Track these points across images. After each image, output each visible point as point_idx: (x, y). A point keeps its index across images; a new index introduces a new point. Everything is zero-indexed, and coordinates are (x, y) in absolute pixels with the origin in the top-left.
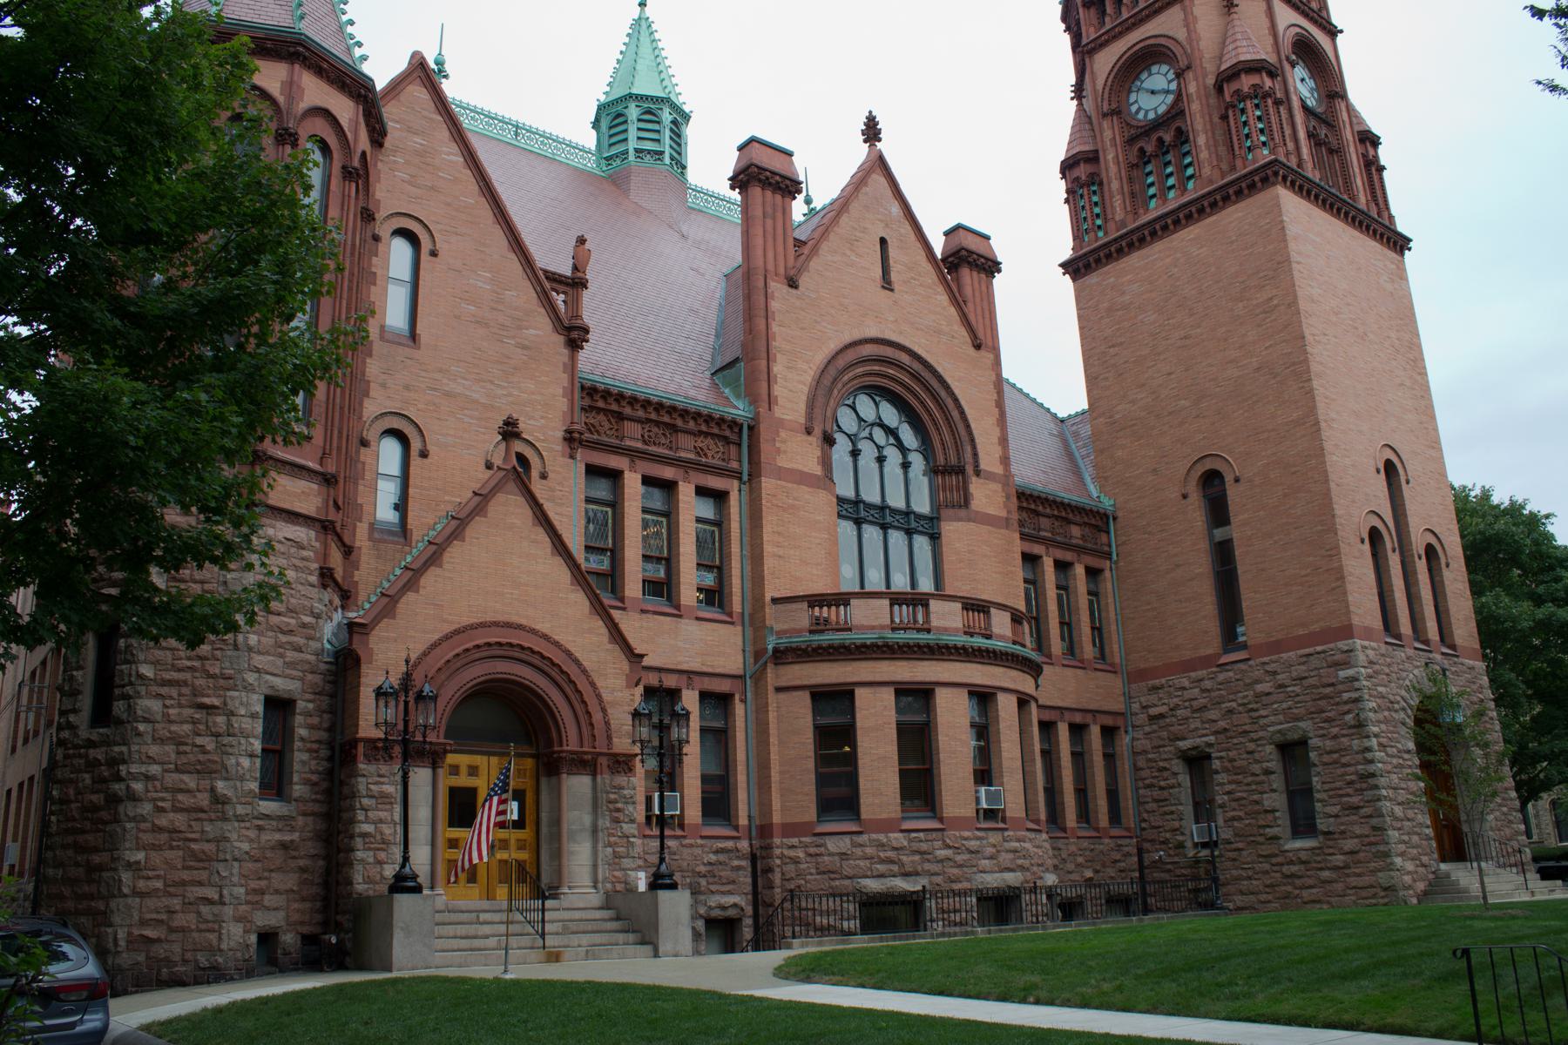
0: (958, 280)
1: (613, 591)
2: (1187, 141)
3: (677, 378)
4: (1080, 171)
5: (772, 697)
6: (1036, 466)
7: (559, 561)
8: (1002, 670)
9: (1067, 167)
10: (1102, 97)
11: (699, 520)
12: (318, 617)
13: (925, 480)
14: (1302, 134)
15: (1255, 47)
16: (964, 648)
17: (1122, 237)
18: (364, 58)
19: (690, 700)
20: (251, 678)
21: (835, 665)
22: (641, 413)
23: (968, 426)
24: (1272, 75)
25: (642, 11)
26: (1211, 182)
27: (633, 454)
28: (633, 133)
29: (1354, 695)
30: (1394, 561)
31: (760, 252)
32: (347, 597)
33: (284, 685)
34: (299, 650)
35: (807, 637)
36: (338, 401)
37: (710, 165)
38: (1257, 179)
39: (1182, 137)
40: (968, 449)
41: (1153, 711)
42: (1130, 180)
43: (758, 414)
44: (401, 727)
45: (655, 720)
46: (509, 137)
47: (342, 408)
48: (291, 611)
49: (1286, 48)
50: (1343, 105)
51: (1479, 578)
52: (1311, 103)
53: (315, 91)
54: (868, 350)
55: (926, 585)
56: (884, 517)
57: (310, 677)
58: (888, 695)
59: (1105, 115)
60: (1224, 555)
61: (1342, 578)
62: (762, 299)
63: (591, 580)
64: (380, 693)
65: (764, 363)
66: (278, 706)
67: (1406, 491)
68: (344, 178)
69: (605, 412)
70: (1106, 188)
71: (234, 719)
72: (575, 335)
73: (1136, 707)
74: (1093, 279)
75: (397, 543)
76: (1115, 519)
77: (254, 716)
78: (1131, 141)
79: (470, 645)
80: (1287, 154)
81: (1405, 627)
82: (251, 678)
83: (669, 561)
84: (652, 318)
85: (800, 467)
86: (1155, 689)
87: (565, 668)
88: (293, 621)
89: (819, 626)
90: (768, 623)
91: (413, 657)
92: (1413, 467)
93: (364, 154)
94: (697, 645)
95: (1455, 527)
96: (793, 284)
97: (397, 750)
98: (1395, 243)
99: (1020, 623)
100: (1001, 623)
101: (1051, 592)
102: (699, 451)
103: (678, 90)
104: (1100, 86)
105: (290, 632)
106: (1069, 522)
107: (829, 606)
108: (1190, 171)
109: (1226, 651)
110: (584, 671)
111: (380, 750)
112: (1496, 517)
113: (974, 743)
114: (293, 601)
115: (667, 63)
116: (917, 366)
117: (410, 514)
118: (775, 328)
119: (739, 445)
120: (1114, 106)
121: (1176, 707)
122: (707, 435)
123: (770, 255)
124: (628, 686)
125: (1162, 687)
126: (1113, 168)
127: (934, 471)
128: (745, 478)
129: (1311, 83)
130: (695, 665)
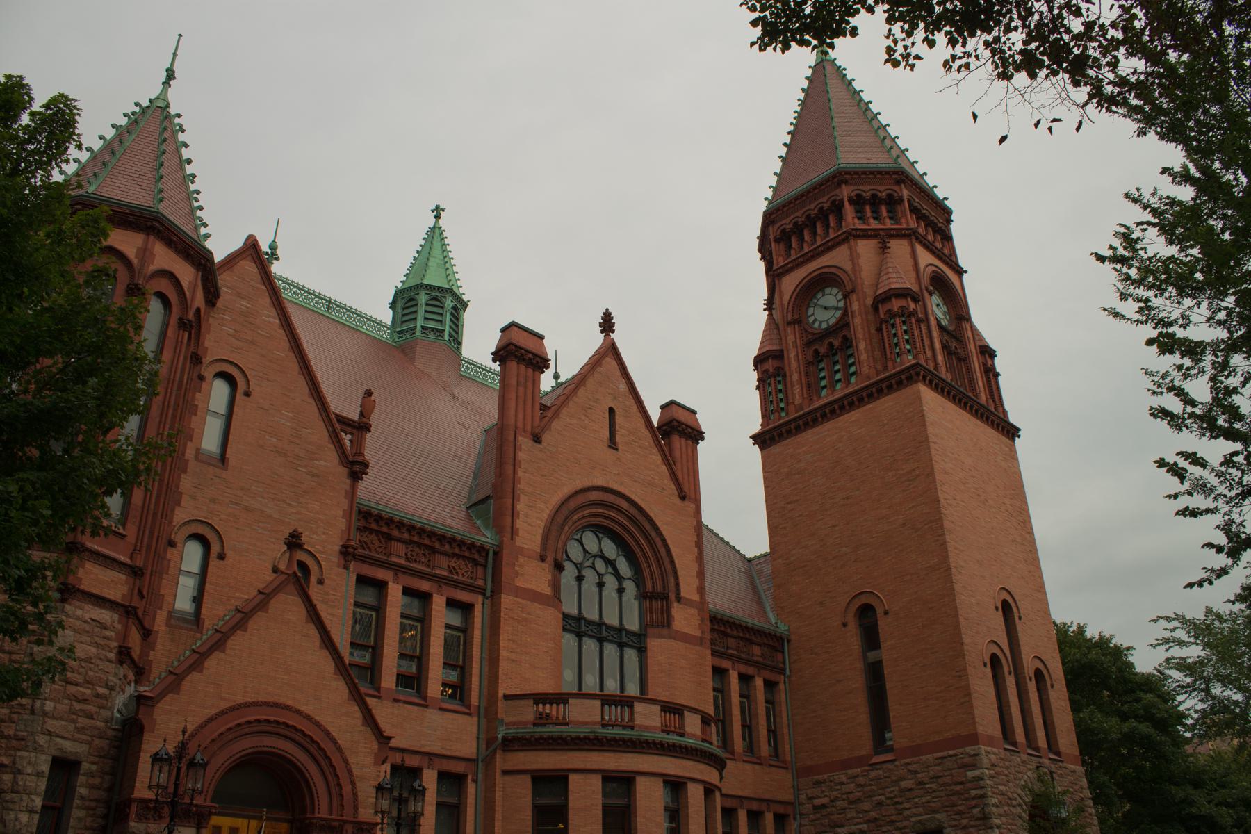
0: (669, 444)
1: (372, 682)
2: (851, 346)
3: (439, 510)
4: (768, 364)
5: (499, 779)
6: (726, 597)
7: (326, 653)
8: (691, 763)
9: (759, 362)
10: (786, 311)
11: (447, 626)
12: (111, 688)
13: (636, 604)
14: (937, 346)
15: (906, 281)
16: (661, 743)
17: (799, 417)
18: (207, 236)
19: (429, 779)
20: (42, 740)
21: (552, 753)
22: (406, 536)
23: (672, 561)
24: (915, 300)
25: (437, 222)
26: (869, 378)
27: (398, 569)
28: (421, 314)
29: (979, 792)
30: (1010, 682)
31: (512, 412)
32: (140, 673)
33: (71, 747)
34: (90, 716)
35: (532, 729)
36: (152, 507)
37: (479, 344)
38: (903, 377)
39: (847, 343)
40: (672, 580)
41: (817, 802)
42: (807, 374)
43: (501, 542)
44: (171, 789)
45: (396, 793)
46: (323, 309)
47: (155, 514)
48: (88, 682)
49: (926, 280)
50: (968, 326)
51: (1078, 697)
52: (944, 322)
53: (163, 257)
54: (595, 496)
55: (632, 689)
56: (600, 632)
57: (97, 741)
58: (596, 781)
59: (789, 323)
60: (875, 674)
61: (969, 694)
62: (511, 450)
63: (354, 673)
64: (156, 758)
65: (509, 501)
66: (64, 767)
67: (1019, 625)
68: (180, 328)
69: (375, 531)
70: (788, 379)
71: (20, 777)
72: (357, 468)
73: (803, 797)
74: (776, 449)
75: (191, 630)
76: (789, 641)
77: (39, 775)
78: (808, 344)
79: (242, 721)
80: (926, 360)
81: (1020, 737)
82: (42, 740)
83: (421, 660)
84: (422, 460)
85: (534, 588)
86: (818, 783)
87: (322, 745)
88: (89, 692)
89: (542, 720)
90: (499, 716)
91: (190, 728)
92: (1024, 606)
93: (198, 310)
94: (441, 732)
95: (1057, 656)
96: (537, 439)
97: (166, 811)
98: (1008, 431)
99: (709, 725)
100: (692, 724)
101: (735, 699)
102: (452, 570)
103: (459, 283)
104: (786, 303)
105: (85, 701)
106: (752, 642)
107: (551, 704)
108: (853, 369)
109: (877, 753)
110: (339, 749)
111: (150, 809)
112: (1089, 649)
113: (666, 824)
114: (91, 673)
115: (453, 262)
116: (633, 511)
117: (204, 606)
118: (520, 473)
119: (485, 567)
120: (796, 317)
121: (836, 799)
122: (459, 556)
123: (520, 416)
124: (376, 764)
125: (824, 782)
126: (794, 364)
127: (643, 596)
128: (488, 593)
129: (944, 308)
130: (436, 748)
